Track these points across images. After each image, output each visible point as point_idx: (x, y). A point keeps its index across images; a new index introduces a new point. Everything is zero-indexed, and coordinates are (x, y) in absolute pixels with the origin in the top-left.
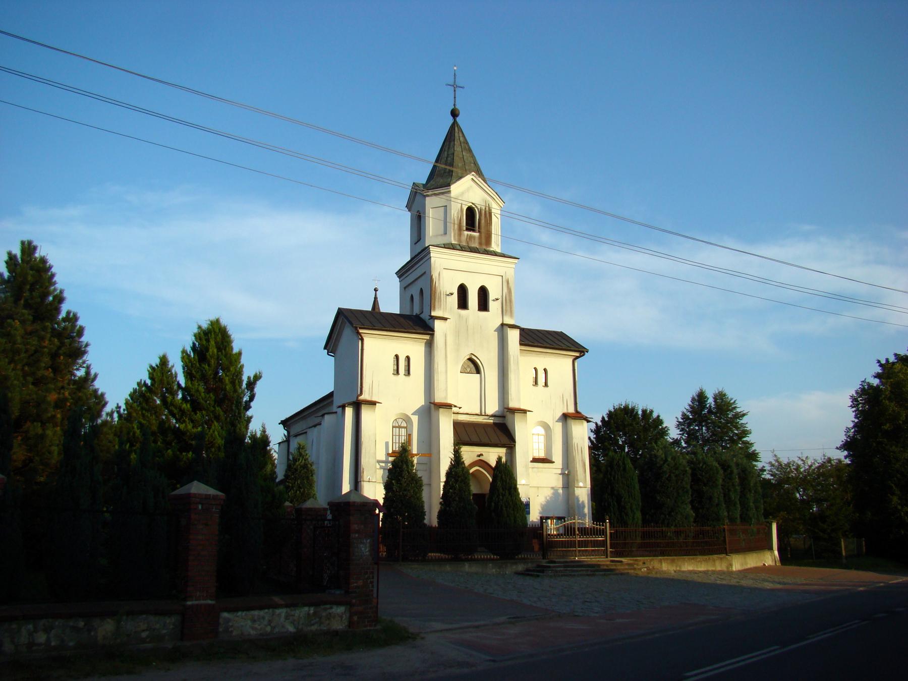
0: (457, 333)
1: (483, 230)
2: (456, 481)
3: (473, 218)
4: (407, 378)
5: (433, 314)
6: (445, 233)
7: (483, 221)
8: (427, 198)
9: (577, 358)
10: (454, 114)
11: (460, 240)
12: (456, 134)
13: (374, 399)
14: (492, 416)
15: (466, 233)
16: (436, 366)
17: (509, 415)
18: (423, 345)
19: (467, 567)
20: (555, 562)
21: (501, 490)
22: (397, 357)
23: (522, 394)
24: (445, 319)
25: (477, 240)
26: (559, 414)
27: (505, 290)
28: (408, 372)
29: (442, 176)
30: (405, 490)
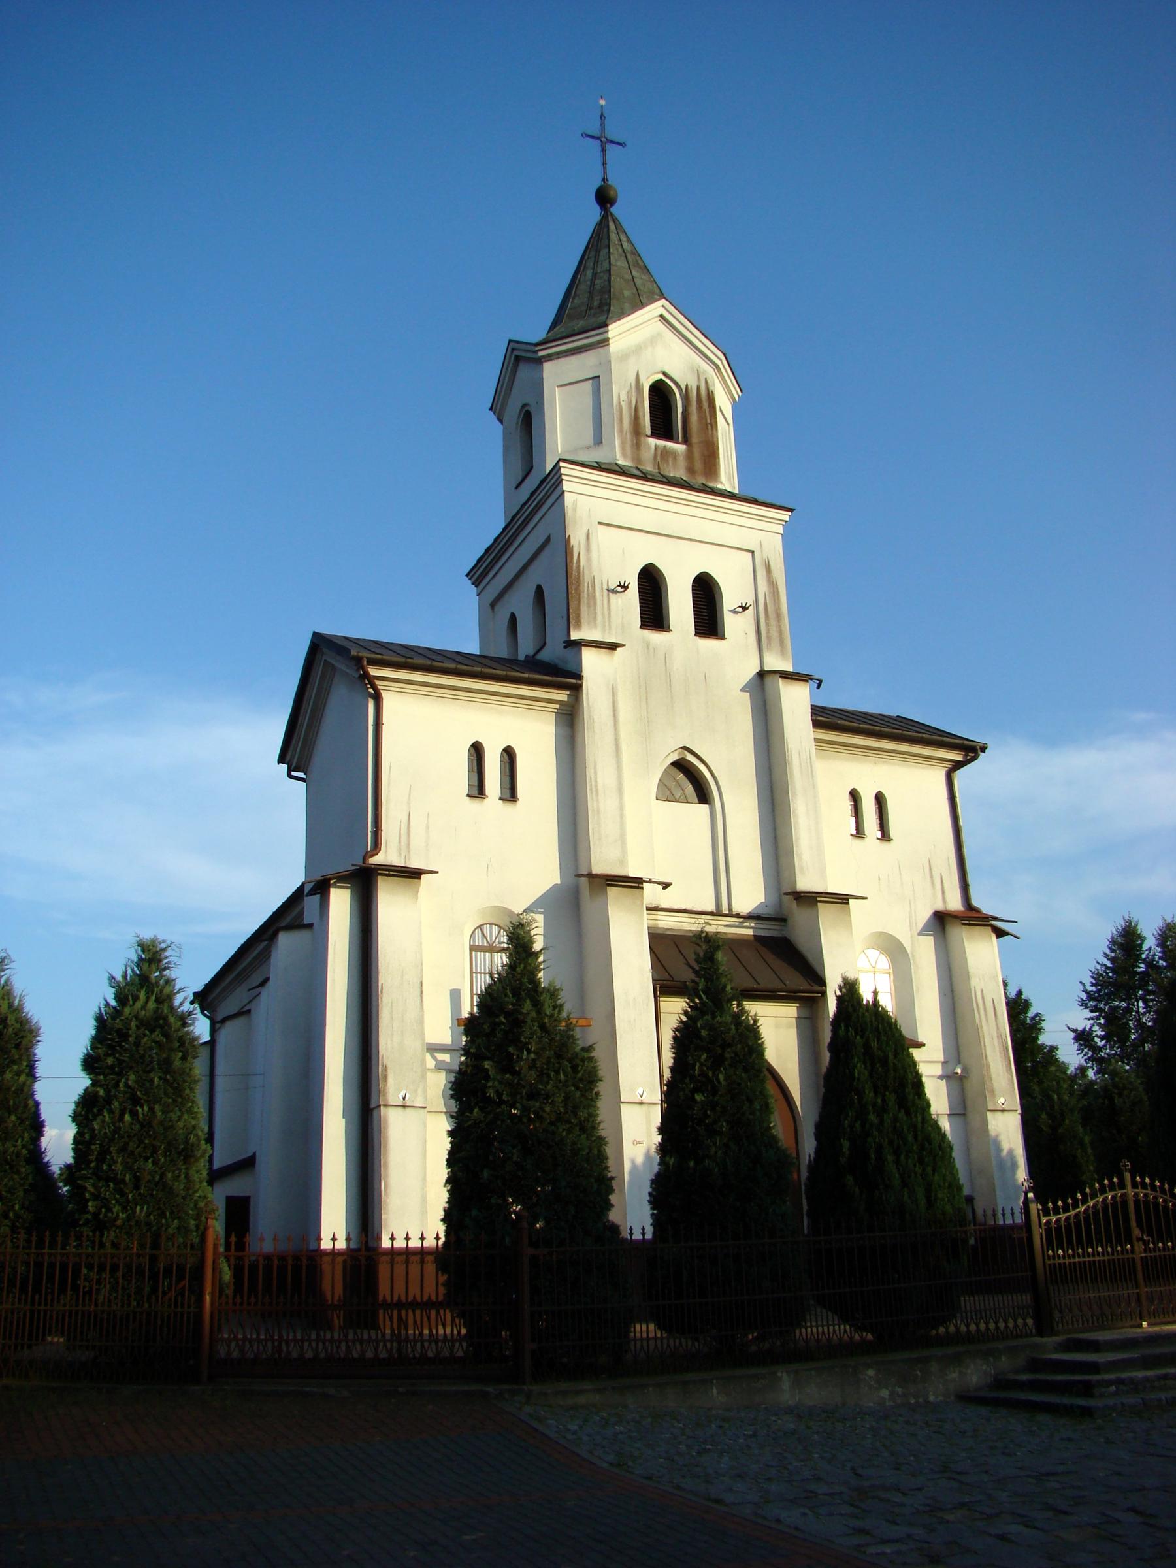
0: (644, 691)
1: (695, 439)
2: (717, 1062)
3: (663, 407)
4: (508, 808)
5: (575, 635)
6: (598, 441)
7: (694, 418)
8: (547, 366)
9: (958, 765)
10: (604, 198)
11: (637, 459)
12: (613, 236)
13: (415, 864)
14: (749, 917)
15: (653, 442)
16: (590, 772)
17: (799, 915)
18: (552, 718)
19: (790, 1390)
20: (1095, 1346)
21: (869, 1095)
22: (477, 751)
23: (828, 855)
24: (612, 647)
25: (682, 463)
26: (925, 914)
27: (763, 587)
28: (510, 793)
29: (587, 308)
30: (532, 1096)
